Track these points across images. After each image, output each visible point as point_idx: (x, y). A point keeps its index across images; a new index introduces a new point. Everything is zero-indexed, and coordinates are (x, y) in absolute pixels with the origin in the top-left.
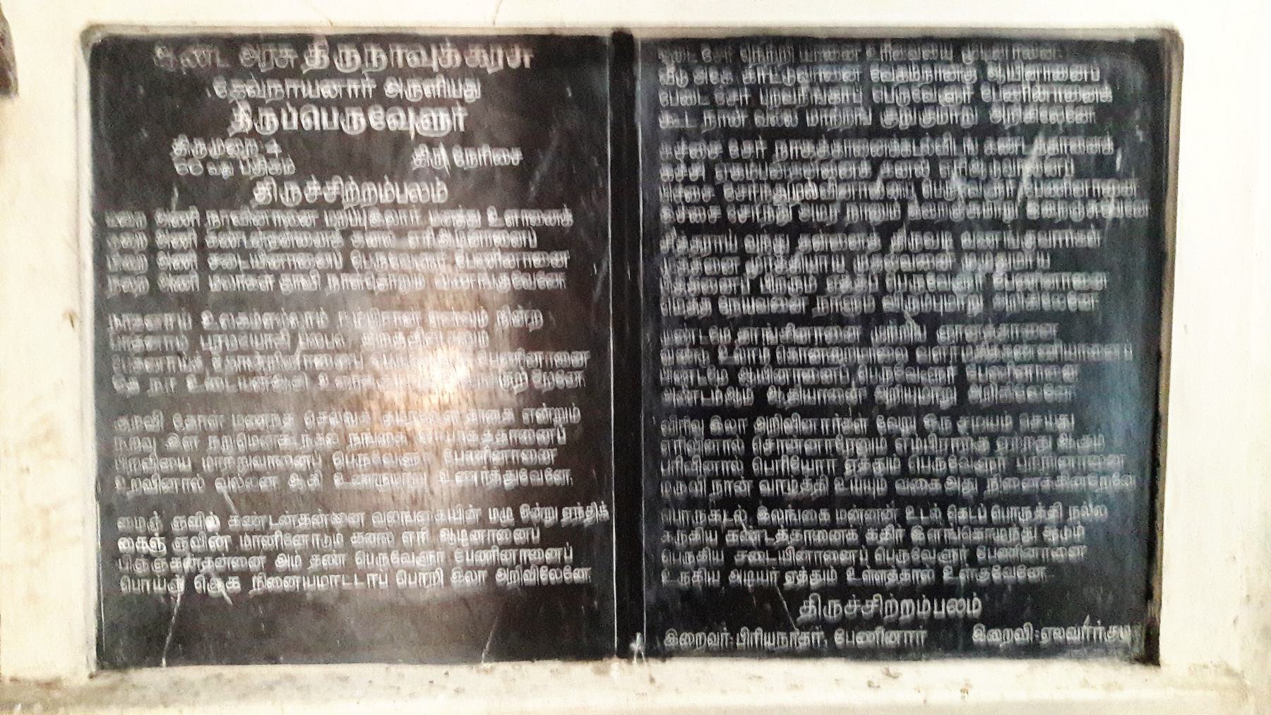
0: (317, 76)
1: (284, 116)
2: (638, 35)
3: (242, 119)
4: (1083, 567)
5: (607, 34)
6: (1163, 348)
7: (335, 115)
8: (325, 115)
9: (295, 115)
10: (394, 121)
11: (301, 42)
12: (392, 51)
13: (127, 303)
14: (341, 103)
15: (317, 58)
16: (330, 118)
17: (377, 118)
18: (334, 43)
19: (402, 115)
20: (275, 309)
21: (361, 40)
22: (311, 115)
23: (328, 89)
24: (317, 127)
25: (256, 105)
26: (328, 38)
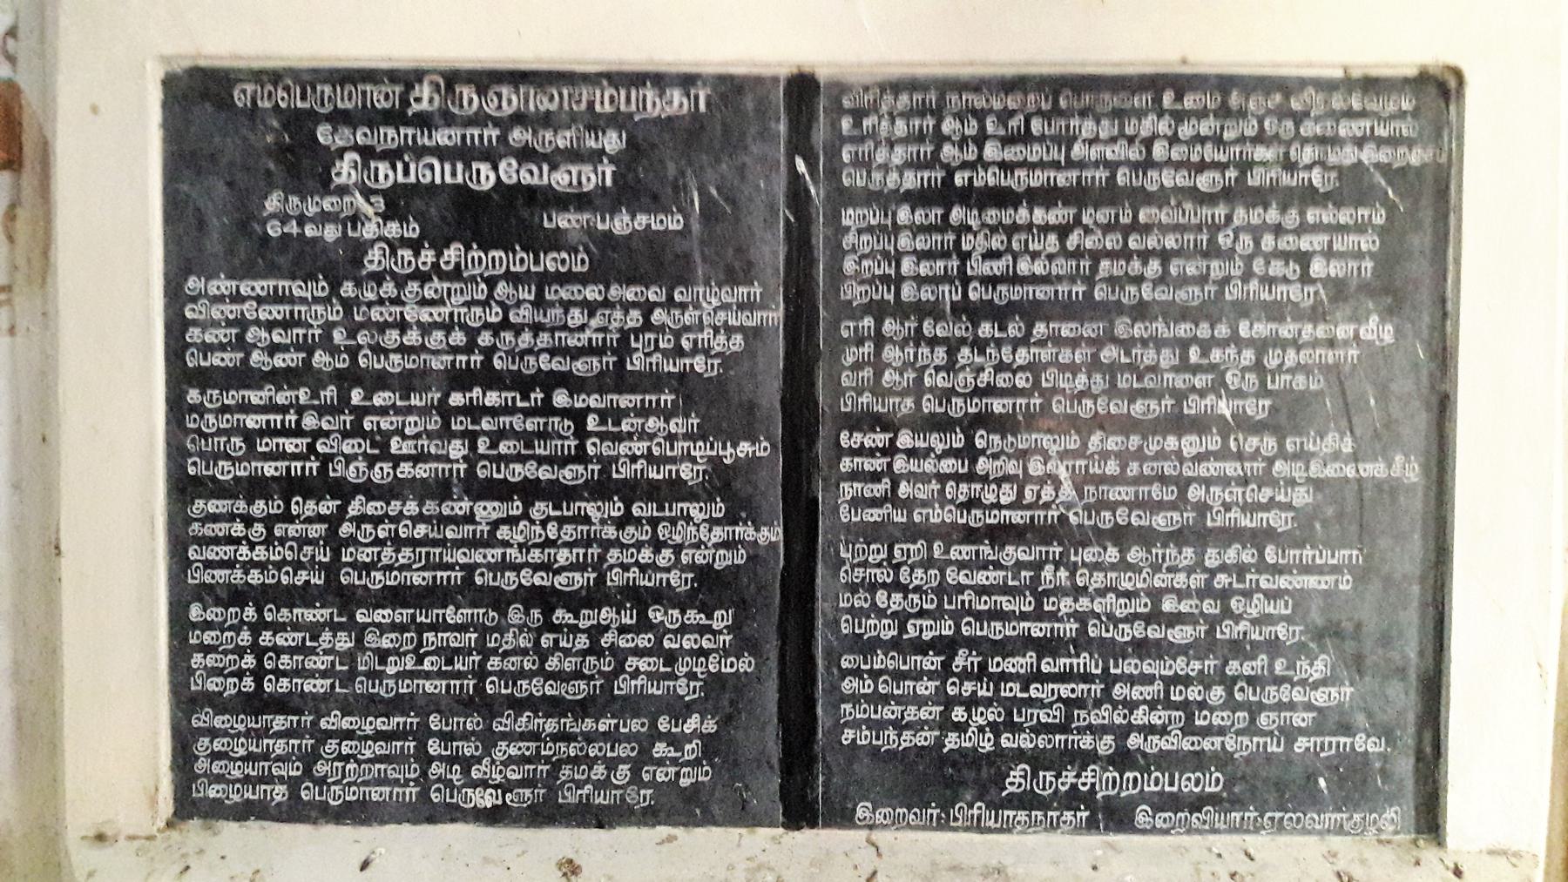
0: (424, 122)
1: (400, 166)
2: (823, 74)
3: (346, 171)
4: (1342, 713)
5: (784, 72)
6: (1441, 822)
7: (460, 167)
8: (447, 167)
9: (412, 167)
10: (528, 176)
11: (408, 78)
12: (692, 92)
13: (203, 378)
14: (463, 154)
15: (425, 98)
16: (454, 174)
17: (509, 171)
18: (452, 79)
19: (535, 169)
20: (1112, 202)
21: (485, 80)
22: (432, 167)
23: (443, 137)
24: (438, 181)
25: (367, 153)
26: (443, 74)
